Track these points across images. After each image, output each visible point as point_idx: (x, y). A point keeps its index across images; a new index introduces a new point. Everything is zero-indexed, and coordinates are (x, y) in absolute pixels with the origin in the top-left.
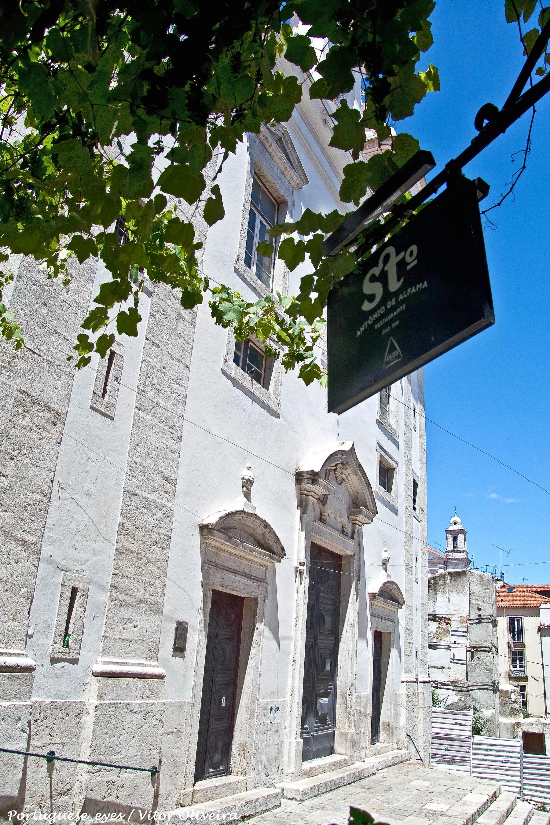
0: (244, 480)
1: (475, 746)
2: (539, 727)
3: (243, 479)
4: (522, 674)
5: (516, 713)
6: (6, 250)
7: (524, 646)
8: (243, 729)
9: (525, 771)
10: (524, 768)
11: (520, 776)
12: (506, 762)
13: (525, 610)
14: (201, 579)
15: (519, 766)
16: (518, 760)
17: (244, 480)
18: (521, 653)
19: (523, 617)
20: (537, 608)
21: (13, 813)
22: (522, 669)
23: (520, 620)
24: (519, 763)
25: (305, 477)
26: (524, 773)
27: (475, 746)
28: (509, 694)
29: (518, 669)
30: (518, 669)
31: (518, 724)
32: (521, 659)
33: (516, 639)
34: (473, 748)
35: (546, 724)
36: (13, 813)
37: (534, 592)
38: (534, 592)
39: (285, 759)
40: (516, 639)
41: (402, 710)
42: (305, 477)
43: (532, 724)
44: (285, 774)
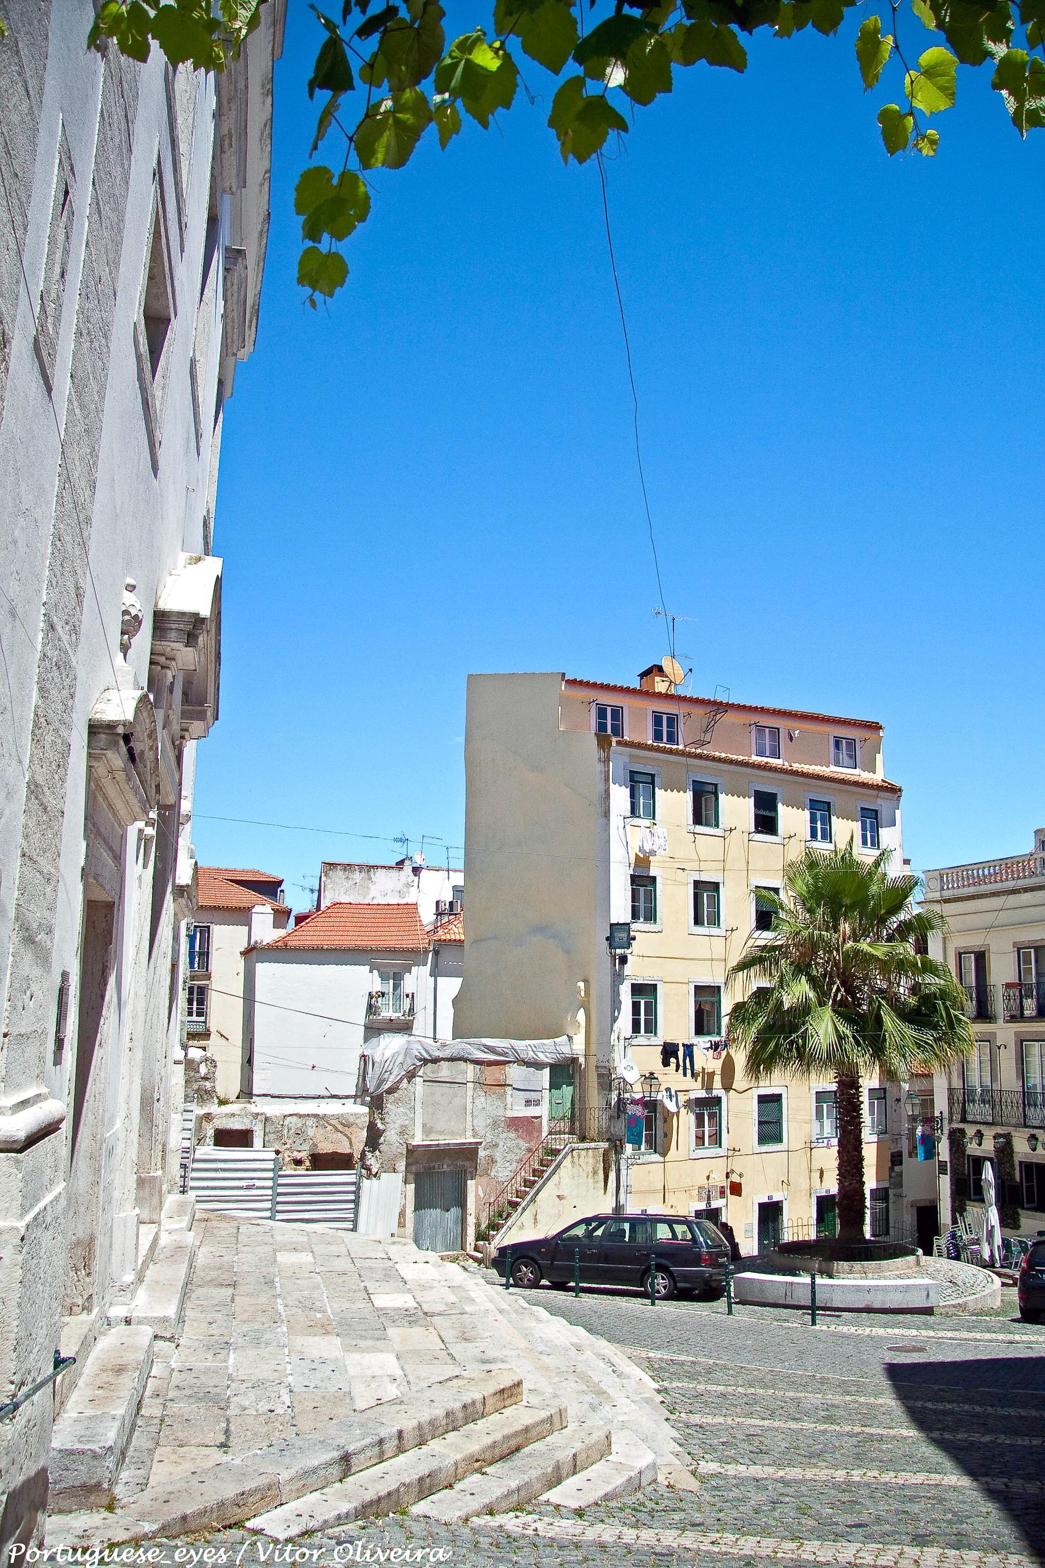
0: (127, 617)
1: (196, 1165)
2: (245, 1120)
3: (126, 612)
4: (200, 1029)
5: (205, 1097)
6: (928, 2)
7: (208, 977)
8: (82, 1209)
9: (279, 1199)
10: (279, 1194)
11: (270, 1209)
12: (248, 1188)
13: (216, 913)
14: (82, 862)
15: (270, 1192)
16: (270, 1183)
17: (127, 617)
18: (202, 991)
19: (212, 926)
20: (249, 910)
21: (19, 1549)
22: (202, 1019)
23: (206, 932)
24: (271, 1188)
25: (174, 626)
26: (278, 1203)
27: (196, 1165)
28: (195, 1065)
29: (194, 1018)
30: (194, 1018)
31: (208, 1117)
32: (201, 1002)
33: (196, 965)
34: (193, 1170)
35: (258, 1114)
36: (19, 1549)
37: (231, 881)
38: (231, 881)
39: (116, 1257)
40: (196, 965)
41: (173, 1116)
42: (174, 626)
43: (233, 1115)
44: (117, 1288)
